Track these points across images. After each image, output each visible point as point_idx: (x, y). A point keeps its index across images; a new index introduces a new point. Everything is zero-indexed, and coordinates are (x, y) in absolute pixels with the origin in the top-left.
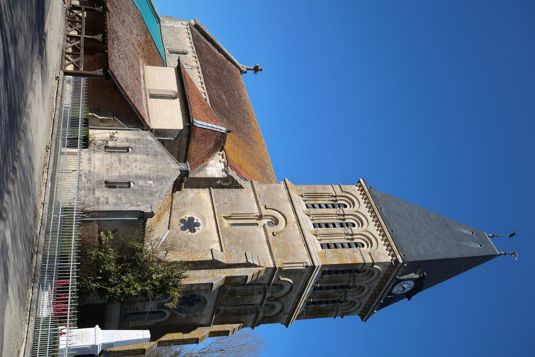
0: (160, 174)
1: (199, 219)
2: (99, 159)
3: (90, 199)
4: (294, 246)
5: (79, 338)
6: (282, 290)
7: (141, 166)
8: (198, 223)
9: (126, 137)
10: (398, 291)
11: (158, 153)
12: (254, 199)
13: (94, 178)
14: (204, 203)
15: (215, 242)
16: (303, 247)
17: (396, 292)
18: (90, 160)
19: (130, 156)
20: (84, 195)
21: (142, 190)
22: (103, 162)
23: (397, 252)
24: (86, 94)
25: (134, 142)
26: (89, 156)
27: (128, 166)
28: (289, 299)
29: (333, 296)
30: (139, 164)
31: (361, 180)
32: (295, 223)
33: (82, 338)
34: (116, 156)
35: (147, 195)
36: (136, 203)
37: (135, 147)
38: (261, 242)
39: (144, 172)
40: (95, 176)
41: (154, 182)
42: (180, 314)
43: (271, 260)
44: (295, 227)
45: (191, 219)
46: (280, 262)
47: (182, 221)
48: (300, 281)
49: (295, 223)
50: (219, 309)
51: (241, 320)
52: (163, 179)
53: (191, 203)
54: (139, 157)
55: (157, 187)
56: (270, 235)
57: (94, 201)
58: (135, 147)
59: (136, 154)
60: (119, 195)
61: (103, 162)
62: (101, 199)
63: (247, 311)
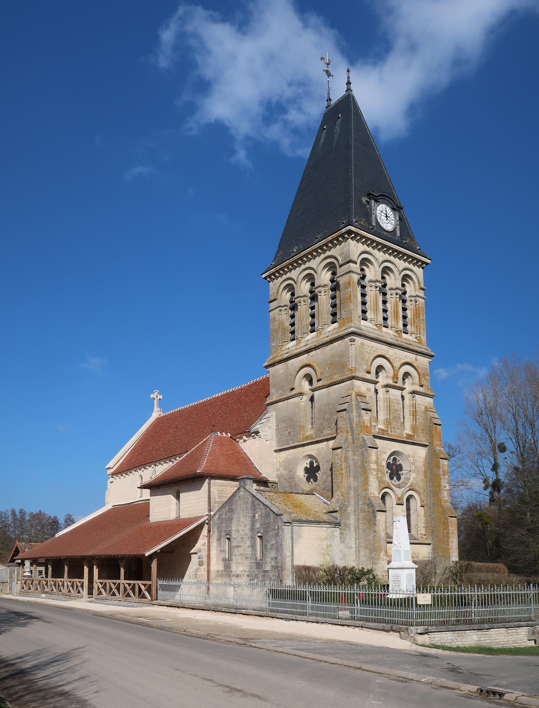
0: (250, 506)
1: (306, 462)
2: (237, 567)
3: (273, 575)
4: (332, 356)
5: (398, 583)
6: (385, 368)
7: (243, 525)
8: (310, 463)
9: (216, 541)
10: (391, 223)
11: (230, 509)
12: (285, 402)
13: (254, 571)
14: (290, 457)
15: (328, 445)
16: (333, 345)
17: (392, 225)
18: (237, 576)
19: (234, 536)
20: (266, 582)
21: (264, 524)
22: (239, 563)
23: (338, 233)
24: (166, 580)
25: (221, 532)
26: (235, 576)
27: (242, 538)
28: (396, 357)
29: (395, 304)
30: (241, 528)
31: (264, 276)
32: (309, 355)
33: (397, 581)
34: (234, 550)
35: (268, 519)
36: (276, 530)
37: (225, 531)
38: (329, 394)
39: (248, 522)
40: (252, 570)
41: (256, 512)
42: (411, 480)
43: (347, 382)
44: (313, 355)
45: (306, 470)
46: (349, 371)
47: (308, 479)
48: (372, 347)
49: (309, 355)
50: (406, 436)
51: (422, 411)
52: (254, 503)
53: (289, 471)
54: (234, 528)
55: (261, 509)
56: (320, 384)
57: (275, 571)
58: (225, 531)
59: (231, 530)
60: (268, 547)
61: (239, 563)
62: (273, 564)
63: (412, 405)
